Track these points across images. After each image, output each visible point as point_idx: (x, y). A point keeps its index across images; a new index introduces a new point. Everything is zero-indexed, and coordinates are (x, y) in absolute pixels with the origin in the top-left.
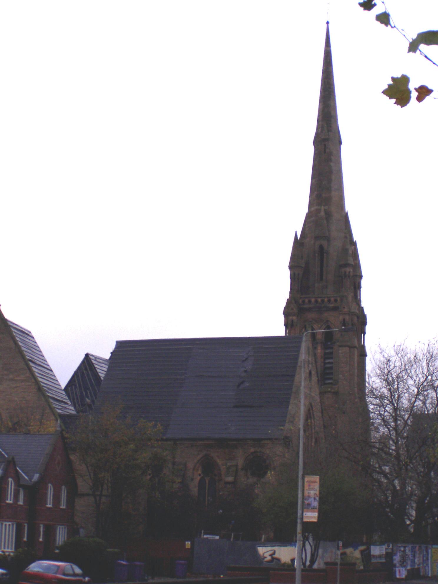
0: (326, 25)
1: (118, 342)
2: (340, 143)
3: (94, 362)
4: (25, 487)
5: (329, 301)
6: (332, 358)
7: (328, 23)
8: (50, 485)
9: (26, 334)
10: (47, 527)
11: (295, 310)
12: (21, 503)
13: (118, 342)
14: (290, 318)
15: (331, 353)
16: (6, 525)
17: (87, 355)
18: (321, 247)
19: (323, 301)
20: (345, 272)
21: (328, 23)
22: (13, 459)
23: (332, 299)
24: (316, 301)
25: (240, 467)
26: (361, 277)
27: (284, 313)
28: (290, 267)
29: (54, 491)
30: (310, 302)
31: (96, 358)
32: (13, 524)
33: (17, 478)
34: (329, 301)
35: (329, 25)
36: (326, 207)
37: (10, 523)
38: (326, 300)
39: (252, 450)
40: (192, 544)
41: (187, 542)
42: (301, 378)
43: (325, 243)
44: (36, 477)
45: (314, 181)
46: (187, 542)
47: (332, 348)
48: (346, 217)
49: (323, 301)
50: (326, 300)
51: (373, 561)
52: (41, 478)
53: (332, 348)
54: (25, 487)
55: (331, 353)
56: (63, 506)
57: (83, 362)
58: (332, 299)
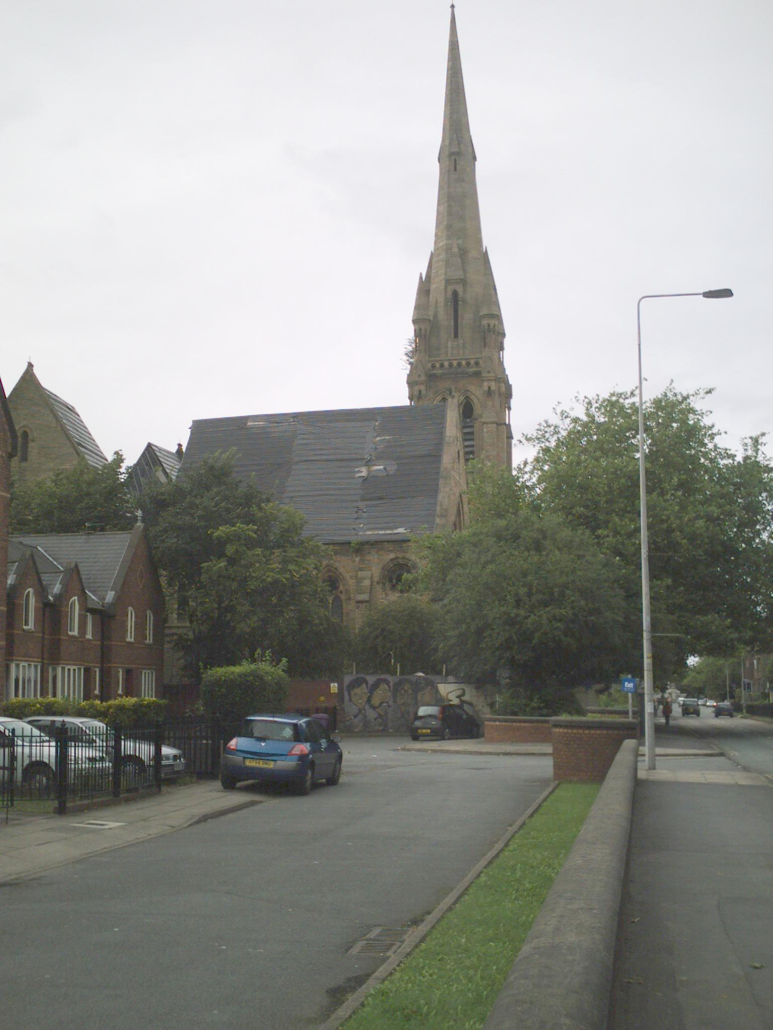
0: (450, 10)
1: (194, 422)
2: (475, 158)
3: (158, 454)
4: (92, 611)
5: (468, 364)
6: (473, 440)
7: (453, 6)
8: (130, 608)
9: (71, 410)
10: (128, 672)
11: (423, 378)
12: (89, 636)
13: (194, 422)
14: (416, 388)
15: (472, 433)
16: (69, 670)
17: (149, 446)
18: (455, 293)
19: (459, 365)
20: (489, 325)
21: (453, 6)
22: (76, 566)
23: (472, 362)
24: (451, 365)
25: (376, 579)
26: (504, 335)
27: (408, 383)
28: (415, 322)
29: (136, 617)
30: (442, 366)
31: (160, 449)
32: (79, 669)
33: (83, 597)
34: (468, 364)
35: (455, 10)
36: (460, 242)
37: (76, 667)
38: (464, 363)
39: (392, 556)
40: (340, 688)
41: (332, 685)
42: (447, 459)
43: (460, 289)
44: (110, 596)
45: (441, 208)
46: (332, 685)
47: (472, 427)
48: (485, 256)
49: (459, 365)
50: (464, 363)
51: (164, 762)
52: (118, 599)
53: (472, 427)
54: (92, 611)
55: (472, 433)
56: (149, 640)
57: (143, 455)
58: (472, 362)
